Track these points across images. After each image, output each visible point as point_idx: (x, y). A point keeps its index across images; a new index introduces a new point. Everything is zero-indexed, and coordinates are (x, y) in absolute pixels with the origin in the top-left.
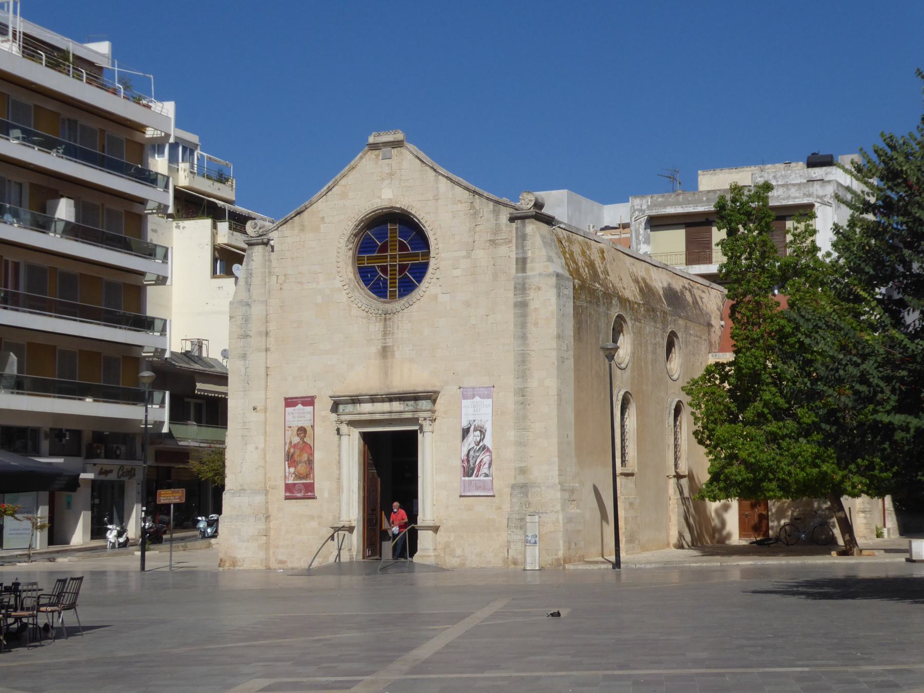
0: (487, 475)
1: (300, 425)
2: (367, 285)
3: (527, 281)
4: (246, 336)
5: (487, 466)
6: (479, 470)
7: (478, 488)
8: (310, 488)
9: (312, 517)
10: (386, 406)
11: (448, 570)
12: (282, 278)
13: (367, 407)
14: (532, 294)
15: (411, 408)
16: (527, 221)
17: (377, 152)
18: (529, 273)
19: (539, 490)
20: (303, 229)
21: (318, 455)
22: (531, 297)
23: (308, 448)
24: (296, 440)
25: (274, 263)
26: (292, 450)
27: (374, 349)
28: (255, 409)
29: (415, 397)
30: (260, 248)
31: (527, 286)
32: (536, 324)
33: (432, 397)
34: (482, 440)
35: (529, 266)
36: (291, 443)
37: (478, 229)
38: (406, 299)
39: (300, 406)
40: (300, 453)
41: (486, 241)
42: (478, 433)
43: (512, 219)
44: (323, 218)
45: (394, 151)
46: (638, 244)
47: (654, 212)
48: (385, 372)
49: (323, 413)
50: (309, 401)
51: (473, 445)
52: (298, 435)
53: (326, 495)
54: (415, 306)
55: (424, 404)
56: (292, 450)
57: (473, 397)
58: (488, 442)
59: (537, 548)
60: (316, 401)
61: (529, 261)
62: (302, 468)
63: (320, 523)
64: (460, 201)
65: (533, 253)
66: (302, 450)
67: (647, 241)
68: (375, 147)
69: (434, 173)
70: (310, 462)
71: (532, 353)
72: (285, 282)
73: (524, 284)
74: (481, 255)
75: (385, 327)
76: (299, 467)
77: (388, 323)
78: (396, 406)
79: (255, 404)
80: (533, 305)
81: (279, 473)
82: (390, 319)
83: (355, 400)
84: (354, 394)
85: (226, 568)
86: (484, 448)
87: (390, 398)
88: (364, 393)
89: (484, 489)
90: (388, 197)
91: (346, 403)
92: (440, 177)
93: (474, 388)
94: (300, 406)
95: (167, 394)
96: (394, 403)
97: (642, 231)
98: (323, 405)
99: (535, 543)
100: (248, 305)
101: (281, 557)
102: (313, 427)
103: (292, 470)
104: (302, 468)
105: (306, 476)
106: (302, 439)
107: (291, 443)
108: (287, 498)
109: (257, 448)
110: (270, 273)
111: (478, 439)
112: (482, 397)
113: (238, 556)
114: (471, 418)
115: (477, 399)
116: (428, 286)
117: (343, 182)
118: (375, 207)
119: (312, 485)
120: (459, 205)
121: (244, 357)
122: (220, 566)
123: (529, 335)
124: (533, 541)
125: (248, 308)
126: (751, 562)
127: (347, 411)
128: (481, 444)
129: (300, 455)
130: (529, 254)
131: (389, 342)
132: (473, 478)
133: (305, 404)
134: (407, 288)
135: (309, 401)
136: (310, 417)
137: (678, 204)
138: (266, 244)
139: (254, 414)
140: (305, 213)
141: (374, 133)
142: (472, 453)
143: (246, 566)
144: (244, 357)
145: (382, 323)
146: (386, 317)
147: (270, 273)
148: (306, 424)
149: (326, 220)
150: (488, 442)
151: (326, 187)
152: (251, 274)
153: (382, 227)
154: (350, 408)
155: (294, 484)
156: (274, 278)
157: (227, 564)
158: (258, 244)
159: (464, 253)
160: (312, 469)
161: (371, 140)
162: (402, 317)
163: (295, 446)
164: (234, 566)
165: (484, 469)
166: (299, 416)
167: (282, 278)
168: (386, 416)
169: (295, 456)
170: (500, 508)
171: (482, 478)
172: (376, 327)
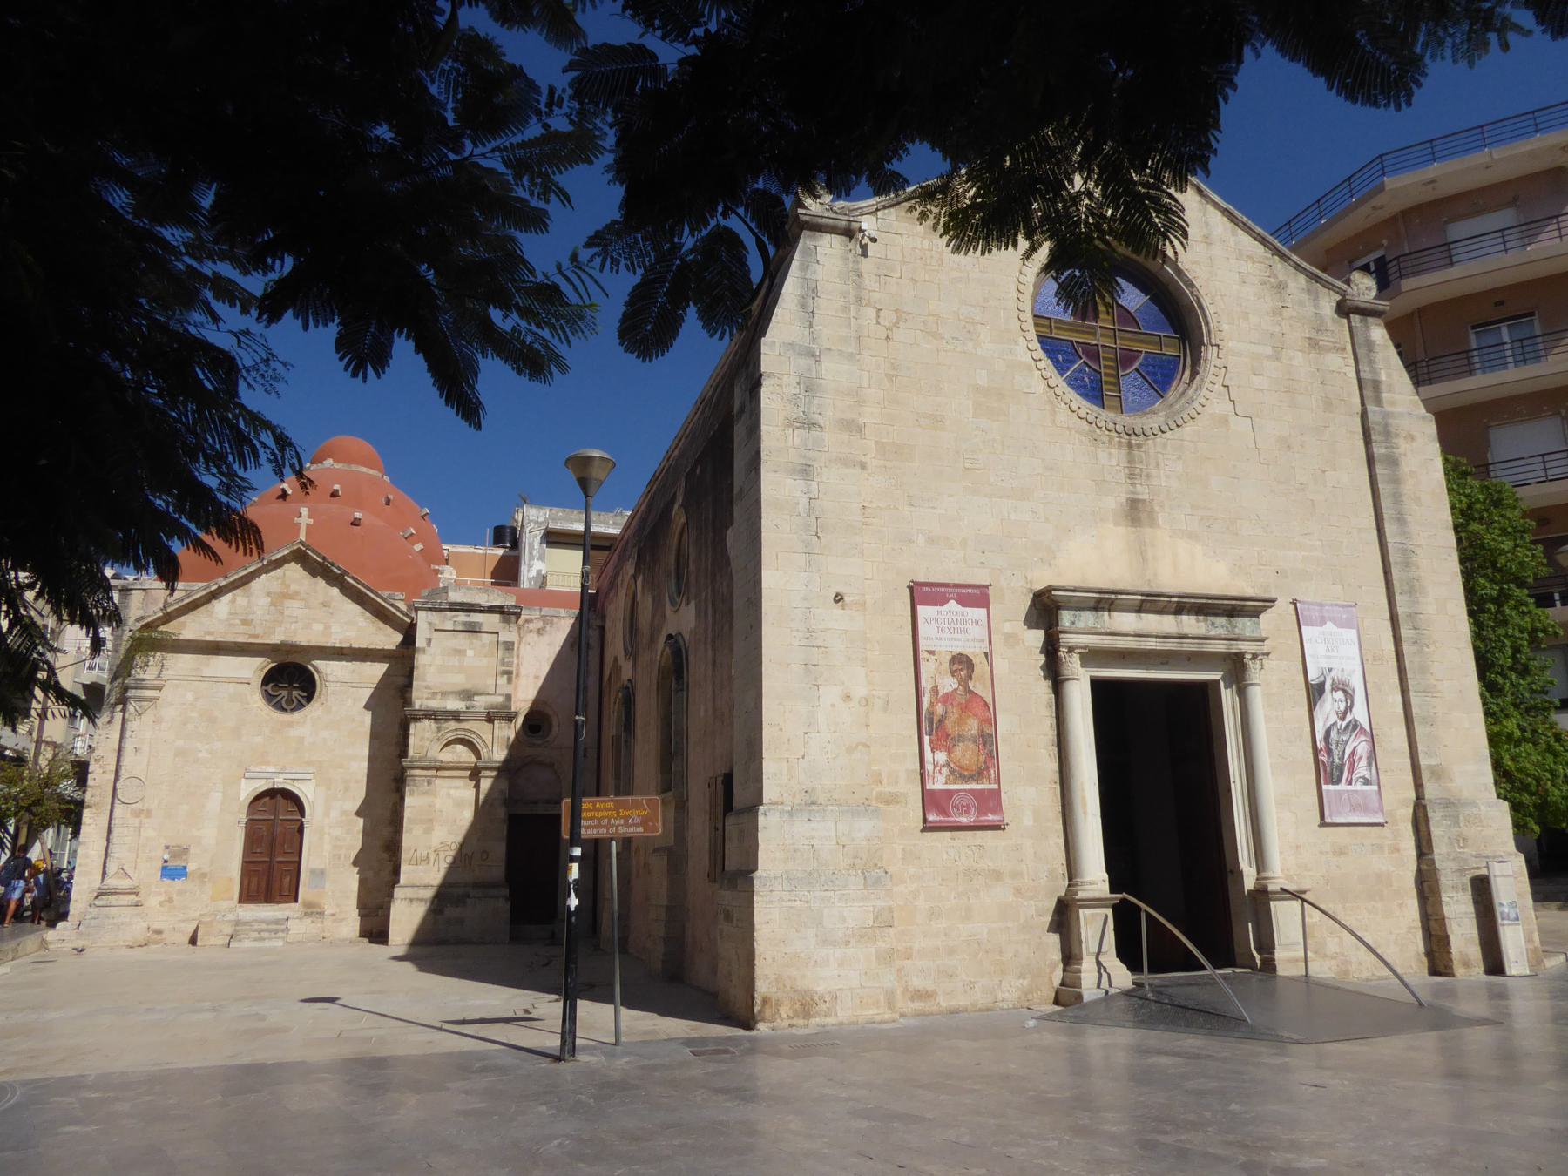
0: (1367, 782)
1: (956, 650)
2: (1061, 369)
3: (1390, 421)
5: (1364, 762)
6: (1351, 771)
7: (1355, 808)
8: (991, 801)
9: (997, 876)
10: (1168, 623)
13: (1126, 621)
15: (1222, 632)
16: (1370, 319)
19: (1475, 811)
21: (1004, 724)
22: (1401, 450)
23: (979, 707)
24: (949, 684)
25: (869, 282)
26: (940, 709)
27: (1114, 501)
30: (836, 240)
31: (1392, 430)
32: (1418, 500)
33: (1273, 601)
34: (1349, 709)
35: (1385, 395)
36: (935, 690)
37: (1286, 313)
39: (953, 605)
40: (952, 718)
42: (1339, 695)
46: (532, 558)
47: (552, 525)
48: (1141, 554)
49: (1007, 627)
50: (976, 596)
51: (1333, 718)
52: (953, 673)
53: (1028, 820)
54: (1187, 429)
55: (1244, 625)
56: (940, 709)
57: (1322, 622)
58: (1359, 713)
60: (991, 592)
61: (1384, 387)
62: (966, 754)
63: (1018, 891)
65: (1389, 375)
66: (965, 708)
67: (542, 558)
69: (1198, 198)
70: (988, 740)
71: (1417, 550)
72: (896, 324)
73: (1386, 425)
74: (1300, 361)
75: (1131, 461)
76: (958, 751)
77: (1136, 452)
78: (1190, 624)
81: (896, 754)
82: (1139, 446)
83: (1105, 602)
84: (1111, 587)
85: (781, 1023)
86: (1354, 725)
87: (1183, 606)
88: (1129, 587)
89: (1366, 810)
91: (1080, 606)
92: (1210, 207)
93: (1321, 605)
94: (953, 605)
96: (1185, 618)
97: (536, 546)
98: (1012, 605)
101: (917, 983)
102: (988, 656)
103: (941, 757)
104: (966, 754)
105: (980, 774)
106: (964, 682)
107: (935, 690)
108: (928, 827)
109: (848, 697)
110: (859, 299)
111: (1342, 707)
112: (1340, 624)
113: (821, 988)
114: (1325, 664)
115: (1329, 626)
119: (996, 794)
121: (805, 471)
123: (1409, 518)
124: (1513, 915)
125: (811, 361)
127: (1080, 625)
128: (1349, 718)
129: (960, 722)
130: (1383, 377)
132: (1343, 786)
133: (965, 601)
135: (976, 596)
136: (980, 632)
137: (606, 524)
138: (849, 233)
139: (837, 610)
142: (1333, 734)
143: (844, 1014)
145: (1124, 452)
146: (1132, 439)
147: (859, 299)
148: (974, 650)
150: (1359, 713)
152: (815, 290)
154: (1087, 619)
155: (950, 793)
156: (872, 312)
157: (785, 1011)
158: (833, 230)
159: (1269, 351)
160: (992, 757)
162: (1164, 446)
163: (947, 698)
164: (807, 1014)
165: (1362, 770)
166: (948, 629)
167: (888, 317)
168: (1171, 645)
169: (949, 724)
170: (1397, 850)
171: (1359, 787)
172: (1111, 458)
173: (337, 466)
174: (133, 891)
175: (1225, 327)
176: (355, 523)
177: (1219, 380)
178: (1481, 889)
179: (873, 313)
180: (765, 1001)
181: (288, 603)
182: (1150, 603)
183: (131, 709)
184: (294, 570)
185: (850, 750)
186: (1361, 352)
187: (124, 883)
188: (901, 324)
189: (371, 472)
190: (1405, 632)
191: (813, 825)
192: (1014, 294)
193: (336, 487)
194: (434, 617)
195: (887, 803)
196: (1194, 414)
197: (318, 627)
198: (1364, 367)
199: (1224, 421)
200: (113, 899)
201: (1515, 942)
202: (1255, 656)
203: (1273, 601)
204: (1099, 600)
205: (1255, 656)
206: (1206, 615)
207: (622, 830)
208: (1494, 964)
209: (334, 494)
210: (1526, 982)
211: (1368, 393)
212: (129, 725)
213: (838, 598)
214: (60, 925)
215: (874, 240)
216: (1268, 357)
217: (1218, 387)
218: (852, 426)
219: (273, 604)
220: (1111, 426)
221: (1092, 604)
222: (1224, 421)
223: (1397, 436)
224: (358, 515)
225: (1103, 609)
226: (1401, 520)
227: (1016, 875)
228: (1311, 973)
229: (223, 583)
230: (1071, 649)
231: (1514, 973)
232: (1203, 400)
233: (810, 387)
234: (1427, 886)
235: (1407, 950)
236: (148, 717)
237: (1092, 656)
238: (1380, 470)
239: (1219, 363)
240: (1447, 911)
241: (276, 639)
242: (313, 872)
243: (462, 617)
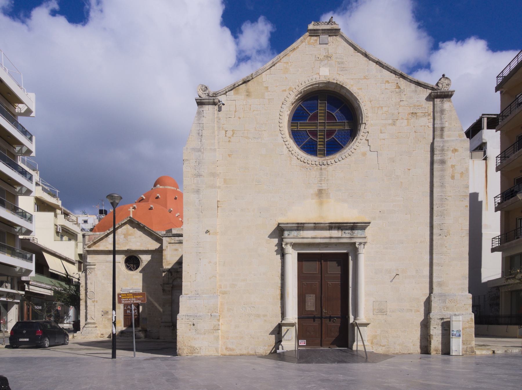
4: (199, 175)
9: (258, 316)
11: (386, 356)
12: (229, 134)
14: (450, 154)
15: (348, 236)
17: (315, 38)
18: (446, 138)
20: (248, 94)
27: (314, 190)
28: (207, 232)
29: (353, 227)
30: (211, 107)
32: (453, 177)
35: (446, 133)
37: (402, 103)
38: (331, 157)
41: (409, 114)
43: (430, 98)
44: (267, 88)
45: (330, 39)
55: (357, 233)
59: (461, 339)
61: (446, 130)
64: (388, 82)
68: (315, 33)
75: (321, 175)
78: (335, 233)
79: (208, 229)
80: (449, 164)
82: (326, 169)
83: (300, 227)
87: (332, 226)
90: (325, 74)
91: (291, 229)
95: (34, 255)
99: (460, 336)
100: (199, 150)
101: (230, 346)
113: (196, 346)
116: (357, 147)
117: (285, 60)
118: (314, 81)
120: (387, 84)
121: (198, 191)
122: (106, 212)
126: (11, 300)
127: (291, 236)
130: (446, 125)
131: (324, 186)
134: (334, 147)
138: (214, 104)
140: (250, 83)
141: (313, 23)
144: (198, 191)
149: (269, 89)
151: (271, 62)
153: (315, 101)
154: (294, 233)
158: (209, 104)
159: (390, 121)
161: (311, 27)
167: (229, 134)
173: (161, 187)
174: (94, 323)
175: (370, 115)
176: (151, 209)
177: (364, 138)
178: (446, 326)
179: (224, 132)
180: (179, 349)
181: (129, 237)
182: (317, 227)
183: (88, 272)
184: (128, 226)
185: (210, 278)
186: (437, 115)
187: (92, 321)
188: (235, 135)
189: (172, 188)
190: (435, 231)
191: (196, 300)
192: (278, 116)
193: (158, 195)
194: (168, 239)
195: (223, 294)
196: (350, 153)
197: (139, 244)
198: (437, 121)
199: (364, 154)
200: (90, 325)
201: (457, 345)
202: (360, 244)
203: (370, 223)
204: (298, 227)
205: (360, 244)
206: (342, 230)
207: (135, 301)
208: (446, 350)
209: (157, 198)
210: (461, 359)
211: (438, 133)
212: (88, 277)
213: (207, 232)
214: (78, 332)
215: (223, 104)
216: (389, 124)
217: (364, 141)
218: (214, 175)
219: (125, 237)
220: (313, 163)
221: (296, 228)
222: (364, 154)
223: (447, 150)
224: (151, 206)
225: (300, 230)
226: (442, 186)
227: (265, 316)
228: (358, 349)
229: (108, 232)
230: (287, 244)
231: (453, 354)
232: (355, 147)
233: (199, 163)
234: (425, 325)
235: (415, 347)
236: (93, 274)
237: (295, 246)
238: (436, 166)
239: (365, 131)
240: (432, 332)
241: (125, 248)
242: (143, 318)
243: (177, 238)
